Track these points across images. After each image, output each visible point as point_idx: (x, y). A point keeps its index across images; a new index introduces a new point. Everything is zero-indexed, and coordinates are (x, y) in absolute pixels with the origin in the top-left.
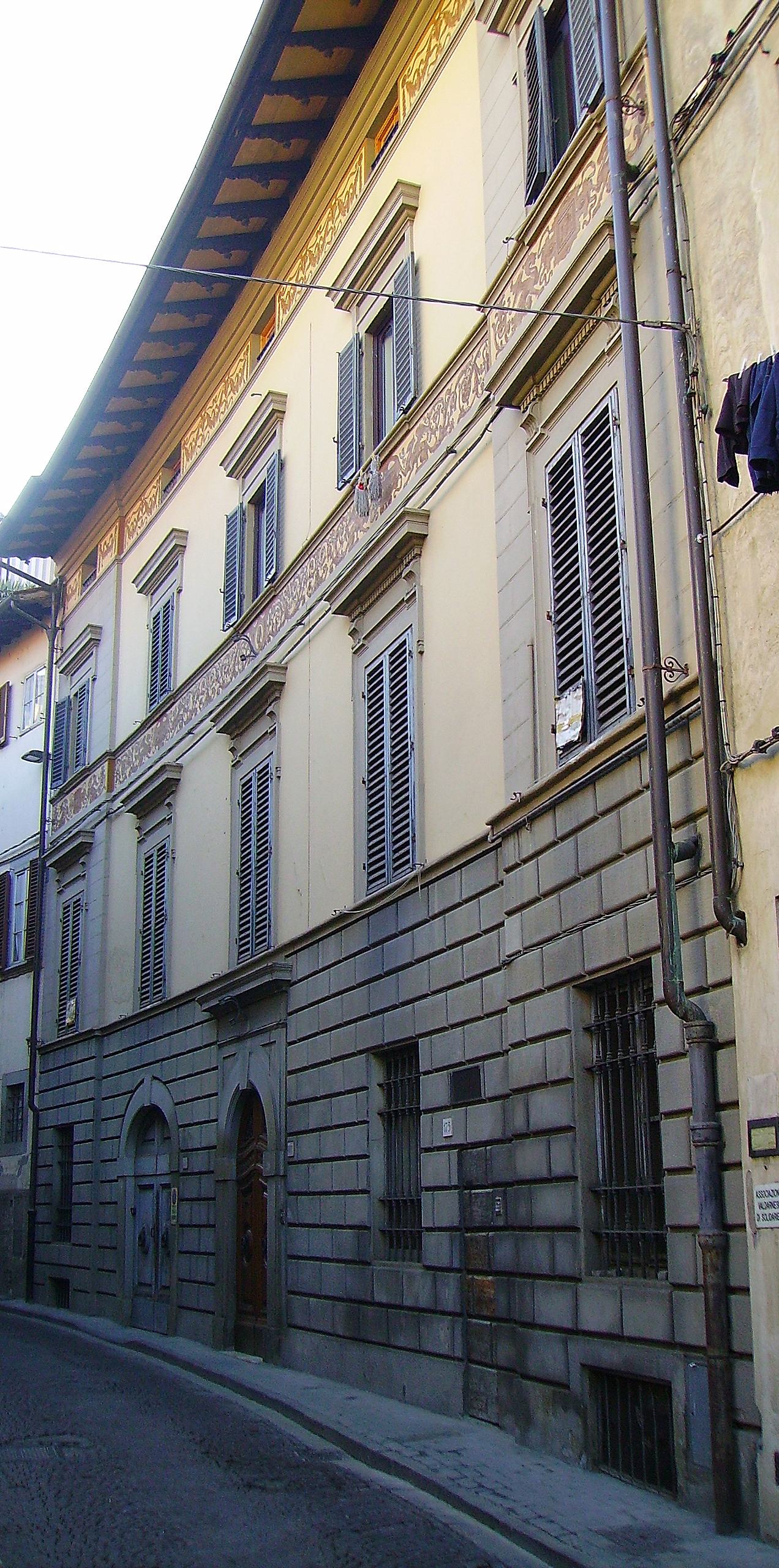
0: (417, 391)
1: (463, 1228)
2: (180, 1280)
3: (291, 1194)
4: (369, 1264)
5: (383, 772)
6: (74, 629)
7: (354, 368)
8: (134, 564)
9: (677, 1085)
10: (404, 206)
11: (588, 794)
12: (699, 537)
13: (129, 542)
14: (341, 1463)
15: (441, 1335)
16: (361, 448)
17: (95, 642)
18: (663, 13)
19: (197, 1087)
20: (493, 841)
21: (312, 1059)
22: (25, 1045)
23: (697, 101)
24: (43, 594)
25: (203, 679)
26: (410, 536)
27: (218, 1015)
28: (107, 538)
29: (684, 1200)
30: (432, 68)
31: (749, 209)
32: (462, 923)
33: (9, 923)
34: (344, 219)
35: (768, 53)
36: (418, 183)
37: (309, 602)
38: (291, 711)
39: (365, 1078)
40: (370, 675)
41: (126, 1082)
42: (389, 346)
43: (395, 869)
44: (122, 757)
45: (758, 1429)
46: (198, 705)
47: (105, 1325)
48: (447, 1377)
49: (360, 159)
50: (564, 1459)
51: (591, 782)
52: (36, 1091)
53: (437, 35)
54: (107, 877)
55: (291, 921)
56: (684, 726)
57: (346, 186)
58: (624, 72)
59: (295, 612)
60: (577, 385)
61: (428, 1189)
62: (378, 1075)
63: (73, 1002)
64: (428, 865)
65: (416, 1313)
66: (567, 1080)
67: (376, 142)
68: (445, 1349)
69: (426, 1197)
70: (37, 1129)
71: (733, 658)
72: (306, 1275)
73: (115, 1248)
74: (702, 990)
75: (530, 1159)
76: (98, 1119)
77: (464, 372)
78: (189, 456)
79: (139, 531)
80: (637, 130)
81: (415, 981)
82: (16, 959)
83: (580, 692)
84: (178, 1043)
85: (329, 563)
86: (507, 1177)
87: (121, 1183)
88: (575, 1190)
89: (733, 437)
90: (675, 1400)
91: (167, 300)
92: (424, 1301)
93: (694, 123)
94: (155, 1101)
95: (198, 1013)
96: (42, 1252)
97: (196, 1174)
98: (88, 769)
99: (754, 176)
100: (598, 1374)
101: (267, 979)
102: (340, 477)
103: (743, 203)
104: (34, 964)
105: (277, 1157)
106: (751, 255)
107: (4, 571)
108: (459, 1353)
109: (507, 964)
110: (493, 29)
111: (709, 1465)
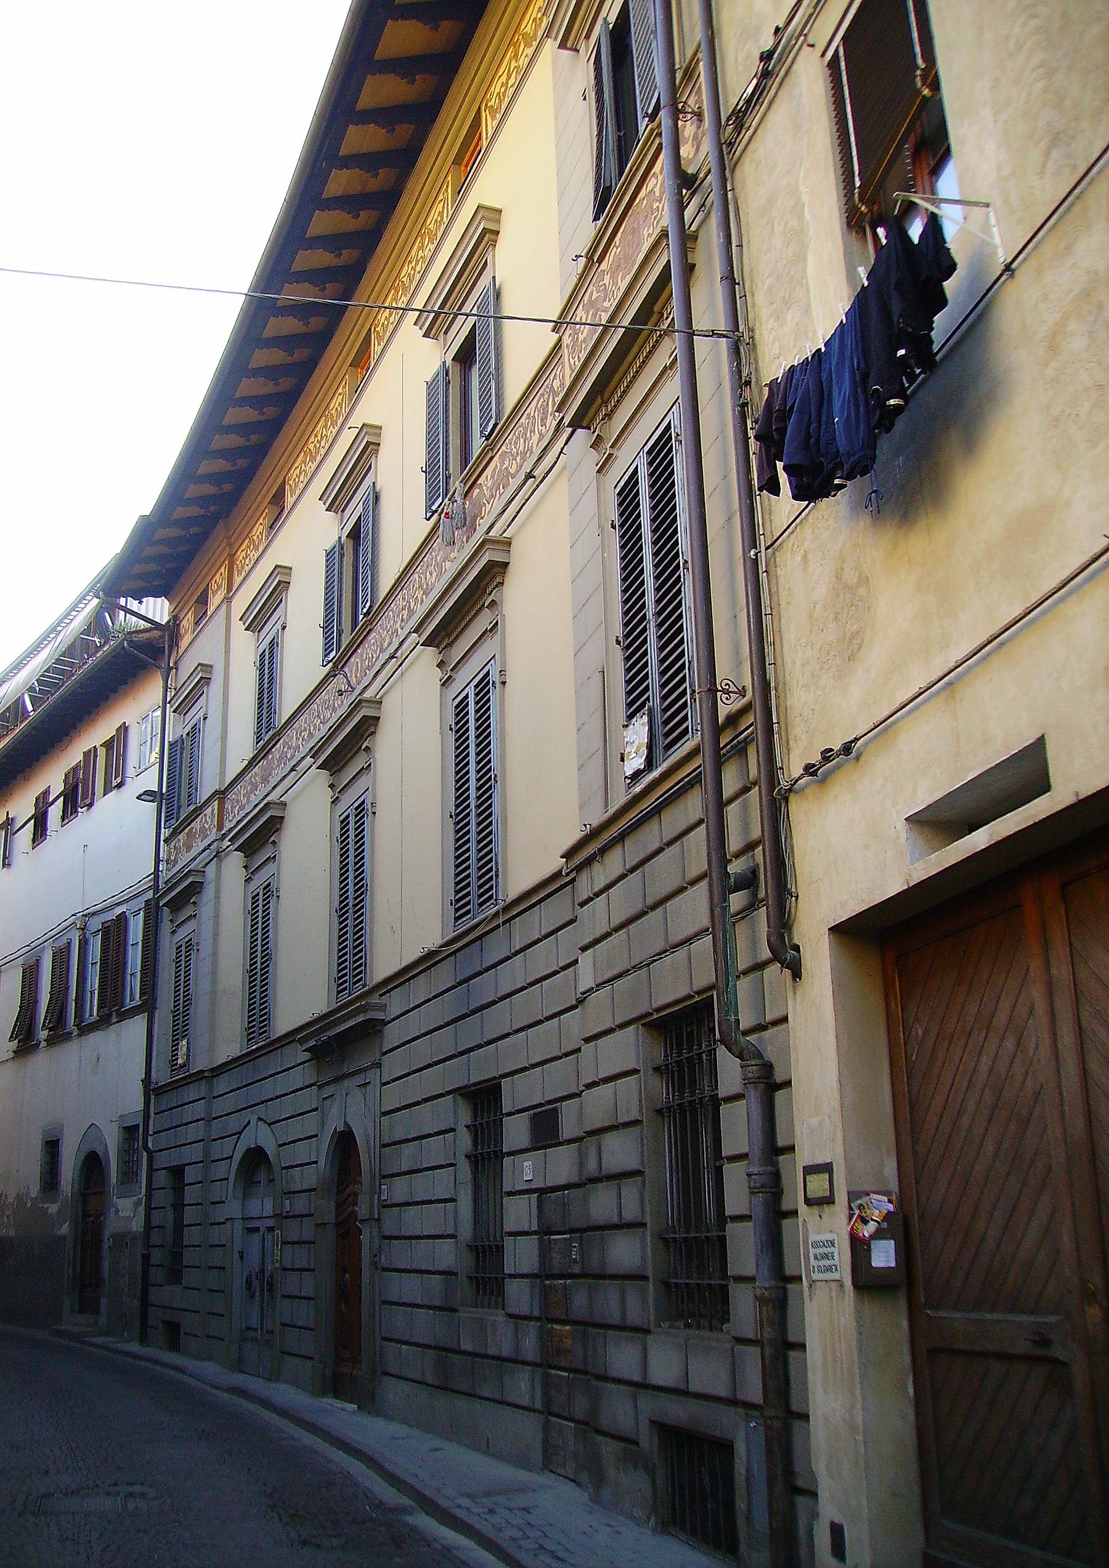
0: (498, 417)
1: (542, 1275)
2: (283, 1325)
3: (385, 1237)
4: (457, 1311)
5: (468, 806)
6: (187, 666)
7: (441, 396)
8: (241, 601)
9: (737, 1127)
10: (485, 231)
11: (653, 824)
12: (752, 553)
13: (237, 580)
14: (410, 1519)
15: (523, 1386)
16: (448, 477)
17: (206, 681)
18: (717, 15)
19: (297, 1127)
20: (567, 874)
21: (402, 1101)
22: (139, 1087)
23: (748, 101)
24: (156, 633)
25: (305, 715)
26: (491, 565)
27: (319, 1054)
28: (217, 577)
29: (744, 1250)
30: (512, 90)
31: (797, 210)
32: (542, 959)
33: (125, 963)
34: (432, 247)
35: (812, 46)
36: (499, 207)
37: (402, 634)
38: (386, 746)
39: (452, 1119)
40: (457, 707)
41: (234, 1123)
42: (475, 372)
43: (481, 905)
44: (231, 796)
45: (814, 1495)
46: (299, 742)
47: (212, 1369)
48: (526, 1429)
49: (447, 190)
50: (634, 1519)
51: (657, 811)
52: (151, 1132)
53: (516, 57)
54: (217, 916)
55: (385, 961)
56: (741, 750)
57: (434, 215)
58: (679, 79)
59: (390, 644)
60: (642, 402)
61: (511, 1234)
62: (465, 1116)
63: (184, 1042)
64: (509, 900)
65: (499, 1363)
66: (636, 1123)
67: (463, 168)
68: (525, 1401)
69: (508, 1242)
70: (151, 1171)
71: (788, 678)
72: (398, 1321)
73: (223, 1292)
74: (761, 1028)
75: (602, 1205)
76: (208, 1161)
77: (543, 395)
78: (293, 492)
79: (247, 569)
80: (695, 137)
81: (498, 1020)
82: (132, 999)
83: (645, 718)
84: (282, 1084)
85: (419, 594)
86: (582, 1223)
87: (229, 1224)
88: (644, 1237)
89: (771, 442)
90: (737, 1461)
91: (264, 335)
92: (506, 1351)
93: (747, 125)
94: (261, 1143)
95: (299, 1053)
96: (156, 1295)
97: (298, 1216)
98: (201, 808)
99: (802, 172)
100: (666, 1431)
101: (361, 1018)
102: (428, 507)
103: (793, 203)
104: (148, 1006)
105: (372, 1199)
106: (800, 257)
107: (122, 613)
108: (538, 1405)
109: (581, 1002)
110: (562, 46)
111: (767, 1531)
